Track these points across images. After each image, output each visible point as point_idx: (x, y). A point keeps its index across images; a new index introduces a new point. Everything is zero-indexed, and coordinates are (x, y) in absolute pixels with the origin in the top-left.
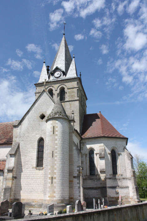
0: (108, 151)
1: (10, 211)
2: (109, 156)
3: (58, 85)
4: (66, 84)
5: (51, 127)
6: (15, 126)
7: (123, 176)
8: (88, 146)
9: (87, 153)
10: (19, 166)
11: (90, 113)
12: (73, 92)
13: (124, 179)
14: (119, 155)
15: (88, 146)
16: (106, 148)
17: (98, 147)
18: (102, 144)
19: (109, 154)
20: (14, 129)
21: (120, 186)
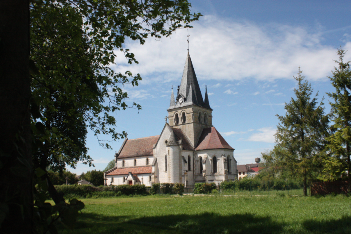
0: (210, 158)
1: (32, 26)
2: (210, 161)
3: (181, 110)
4: (186, 110)
5: (324, 219)
6: (154, 148)
7: (220, 174)
8: (199, 155)
9: (199, 159)
10: (157, 170)
11: (226, 141)
12: (190, 116)
13: (220, 175)
14: (218, 160)
15: (199, 155)
16: (208, 156)
17: (203, 156)
18: (206, 154)
19: (211, 160)
20: (154, 150)
21: (237, 189)
